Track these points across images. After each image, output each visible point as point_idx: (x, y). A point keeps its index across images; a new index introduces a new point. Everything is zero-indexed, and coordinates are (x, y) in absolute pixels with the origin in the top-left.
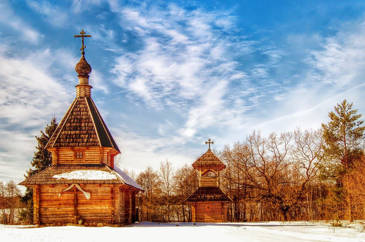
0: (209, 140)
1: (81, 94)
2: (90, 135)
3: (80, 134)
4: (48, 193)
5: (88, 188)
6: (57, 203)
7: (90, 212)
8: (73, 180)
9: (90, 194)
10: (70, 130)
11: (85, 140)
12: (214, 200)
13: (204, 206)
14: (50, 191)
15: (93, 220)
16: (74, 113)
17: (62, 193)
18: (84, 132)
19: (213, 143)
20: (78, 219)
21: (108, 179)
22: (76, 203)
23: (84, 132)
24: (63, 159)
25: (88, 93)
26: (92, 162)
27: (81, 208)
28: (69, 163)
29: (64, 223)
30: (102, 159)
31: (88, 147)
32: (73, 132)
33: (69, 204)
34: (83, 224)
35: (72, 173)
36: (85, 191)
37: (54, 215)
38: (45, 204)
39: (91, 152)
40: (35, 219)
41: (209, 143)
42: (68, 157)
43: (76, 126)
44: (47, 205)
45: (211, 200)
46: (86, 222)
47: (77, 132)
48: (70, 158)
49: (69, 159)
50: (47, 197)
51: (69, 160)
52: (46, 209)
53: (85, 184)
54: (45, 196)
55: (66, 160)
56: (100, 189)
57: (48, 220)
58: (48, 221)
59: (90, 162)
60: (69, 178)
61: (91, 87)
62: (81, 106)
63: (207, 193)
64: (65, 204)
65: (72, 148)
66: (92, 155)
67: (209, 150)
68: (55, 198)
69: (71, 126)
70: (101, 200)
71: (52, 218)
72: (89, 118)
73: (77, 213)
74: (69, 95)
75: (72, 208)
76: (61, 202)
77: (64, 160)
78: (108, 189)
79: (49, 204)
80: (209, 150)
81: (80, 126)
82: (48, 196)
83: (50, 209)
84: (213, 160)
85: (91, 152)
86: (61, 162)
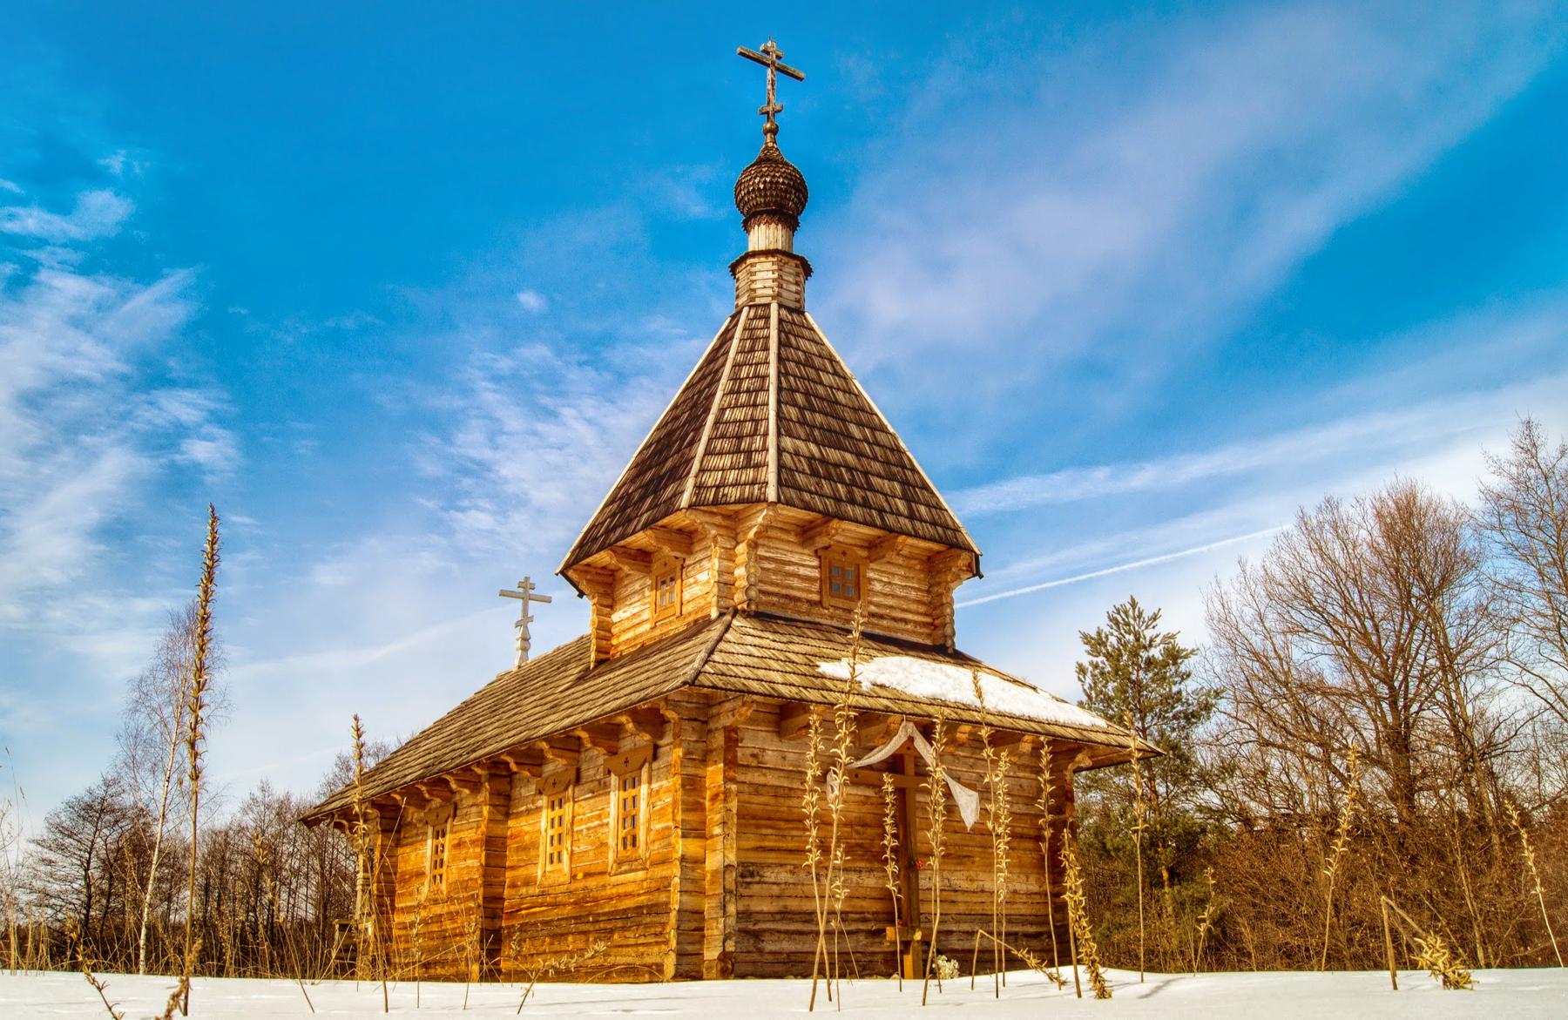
1: (785, 294)
4: (759, 768)
7: (962, 908)
9: (981, 799)
14: (771, 758)
21: (83, 793)
24: (772, 584)
26: (896, 630)
28: (799, 612)
37: (792, 920)
39: (893, 574)
42: (796, 583)
44: (757, 849)
48: (802, 590)
49: (799, 589)
50: (757, 793)
51: (798, 599)
55: (784, 592)
57: (760, 951)
58: (756, 956)
59: (888, 628)
66: (898, 592)
71: (779, 941)
77: (776, 595)
79: (767, 844)
82: (763, 791)
83: (770, 876)
85: (893, 574)
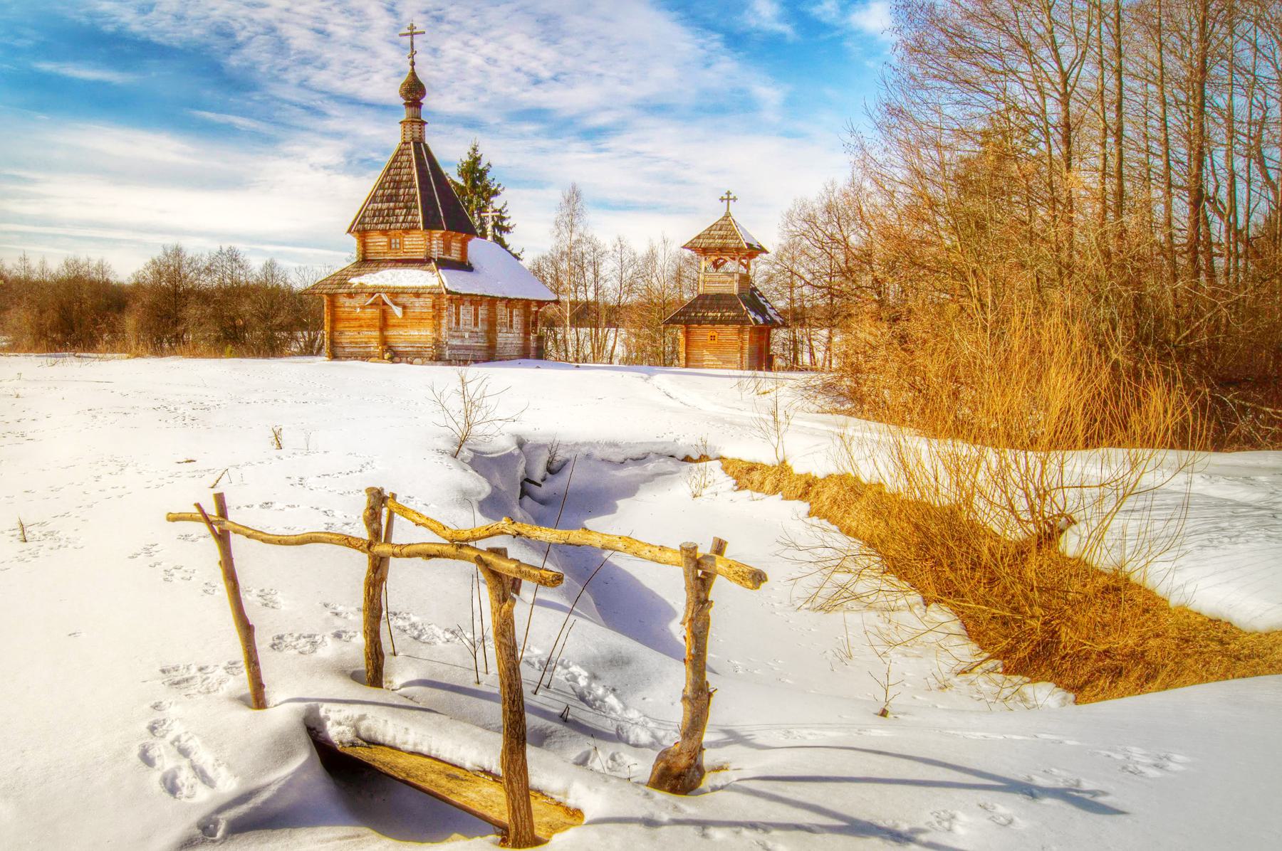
0: (728, 193)
2: (408, 208)
3: (394, 209)
5: (401, 299)
6: (357, 323)
8: (375, 287)
10: (382, 202)
11: (401, 219)
12: (721, 322)
13: (703, 334)
15: (407, 354)
16: (392, 172)
17: (363, 308)
18: (402, 205)
19: (735, 199)
20: (383, 352)
22: (384, 322)
23: (402, 205)
25: (417, 135)
27: (391, 333)
29: (366, 357)
30: (429, 249)
31: (407, 231)
32: (385, 206)
33: (373, 326)
34: (391, 359)
35: (377, 275)
36: (396, 304)
38: (340, 326)
40: (532, 353)
41: (728, 199)
43: (391, 195)
45: (714, 321)
46: (395, 356)
47: (392, 205)
52: (341, 333)
53: (395, 293)
54: (342, 312)
56: (418, 302)
60: (370, 284)
61: (424, 123)
62: (405, 158)
63: (711, 308)
64: (369, 326)
65: (384, 232)
67: (727, 216)
68: (354, 315)
69: (383, 195)
70: (420, 319)
72: (412, 180)
73: (384, 342)
74: (701, 51)
75: (377, 334)
76: (362, 322)
78: (429, 301)
80: (727, 216)
81: (397, 195)
84: (726, 237)
86: (370, 257)
